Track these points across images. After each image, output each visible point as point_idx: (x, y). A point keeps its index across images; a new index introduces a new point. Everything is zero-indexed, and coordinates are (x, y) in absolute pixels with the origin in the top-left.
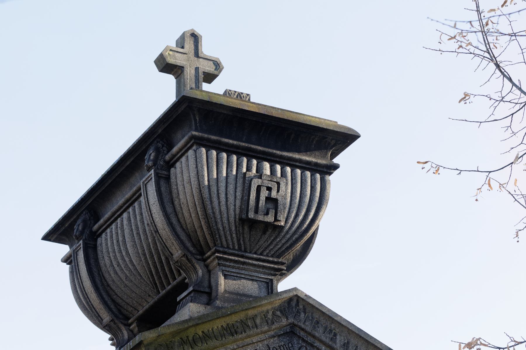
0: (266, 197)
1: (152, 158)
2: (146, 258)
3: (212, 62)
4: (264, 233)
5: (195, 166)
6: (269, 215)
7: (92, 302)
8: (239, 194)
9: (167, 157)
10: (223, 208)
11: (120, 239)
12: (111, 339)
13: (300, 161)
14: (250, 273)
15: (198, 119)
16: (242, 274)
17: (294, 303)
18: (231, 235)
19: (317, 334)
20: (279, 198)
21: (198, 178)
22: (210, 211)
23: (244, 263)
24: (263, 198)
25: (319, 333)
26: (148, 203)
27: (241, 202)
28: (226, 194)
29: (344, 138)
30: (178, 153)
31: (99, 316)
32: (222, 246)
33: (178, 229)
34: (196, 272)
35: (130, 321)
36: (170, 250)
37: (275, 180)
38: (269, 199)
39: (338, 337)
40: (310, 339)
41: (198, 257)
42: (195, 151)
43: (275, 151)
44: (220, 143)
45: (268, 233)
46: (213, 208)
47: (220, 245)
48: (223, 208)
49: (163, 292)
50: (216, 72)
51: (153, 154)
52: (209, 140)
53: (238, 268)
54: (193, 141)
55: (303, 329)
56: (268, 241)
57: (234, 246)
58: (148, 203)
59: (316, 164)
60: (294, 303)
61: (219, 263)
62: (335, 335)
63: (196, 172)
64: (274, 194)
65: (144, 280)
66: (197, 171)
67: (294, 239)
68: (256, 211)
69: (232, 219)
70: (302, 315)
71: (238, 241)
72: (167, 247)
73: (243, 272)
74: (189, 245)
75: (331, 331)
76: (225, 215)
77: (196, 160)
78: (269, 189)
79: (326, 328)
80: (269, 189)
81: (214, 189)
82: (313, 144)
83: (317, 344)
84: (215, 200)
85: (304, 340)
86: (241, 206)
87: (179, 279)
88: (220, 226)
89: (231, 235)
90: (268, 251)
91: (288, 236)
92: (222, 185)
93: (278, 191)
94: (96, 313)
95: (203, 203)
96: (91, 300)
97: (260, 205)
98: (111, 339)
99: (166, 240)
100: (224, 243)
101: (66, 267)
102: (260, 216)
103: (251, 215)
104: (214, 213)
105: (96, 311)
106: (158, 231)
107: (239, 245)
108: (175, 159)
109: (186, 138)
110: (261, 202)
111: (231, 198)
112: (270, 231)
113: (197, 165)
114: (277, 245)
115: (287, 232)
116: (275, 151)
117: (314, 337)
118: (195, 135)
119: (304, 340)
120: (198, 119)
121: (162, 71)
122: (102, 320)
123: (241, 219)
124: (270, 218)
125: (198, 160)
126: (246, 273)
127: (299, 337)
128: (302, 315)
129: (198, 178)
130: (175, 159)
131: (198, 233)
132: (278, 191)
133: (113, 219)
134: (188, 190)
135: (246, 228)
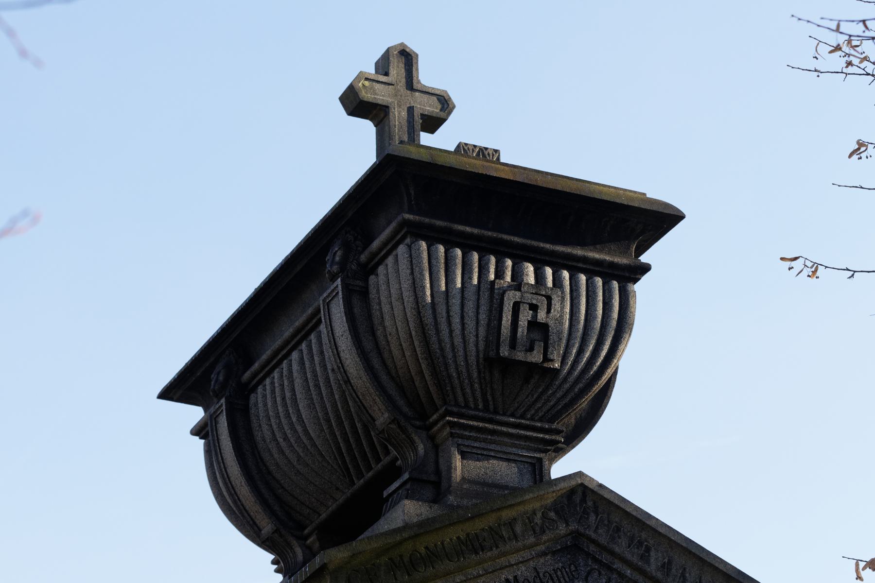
0: (529, 322)
1: (337, 259)
3: (435, 98)
5: (409, 271)
6: (535, 352)
10: (458, 340)
11: (288, 395)
13: (585, 260)
14: (504, 449)
15: (413, 192)
16: (491, 450)
17: (577, 499)
18: (472, 386)
19: (617, 549)
20: (551, 323)
21: (415, 292)
22: (435, 347)
23: (493, 432)
24: (523, 323)
25: (621, 547)
28: (462, 318)
29: (660, 220)
30: (380, 249)
31: (255, 523)
32: (457, 404)
33: (384, 378)
34: (415, 449)
35: (306, 531)
38: (533, 324)
39: (652, 553)
40: (605, 558)
41: (418, 423)
44: (450, 231)
46: (440, 341)
47: (453, 403)
48: (458, 340)
51: (339, 253)
52: (431, 227)
55: (594, 541)
56: (533, 396)
57: (476, 405)
59: (612, 265)
60: (577, 499)
61: (451, 433)
62: (648, 550)
64: (542, 316)
66: (414, 279)
67: (576, 390)
68: (513, 345)
69: (472, 359)
70: (592, 518)
71: (484, 395)
72: (365, 408)
73: (492, 447)
74: (401, 402)
75: (640, 543)
76: (461, 353)
77: (411, 261)
78: (534, 308)
79: (632, 539)
80: (534, 308)
81: (442, 309)
82: (614, 232)
83: (617, 565)
84: (444, 327)
85: (595, 560)
86: (487, 337)
88: (452, 371)
89: (472, 386)
90: (533, 412)
91: (567, 386)
92: (456, 302)
93: (549, 311)
94: (249, 519)
96: (241, 497)
99: (363, 395)
100: (461, 399)
101: (199, 444)
103: (505, 352)
104: (442, 349)
105: (249, 515)
109: (394, 225)
111: (470, 324)
113: (412, 269)
114: (548, 400)
115: (565, 379)
117: (612, 553)
119: (595, 560)
120: (413, 192)
122: (260, 530)
123: (487, 359)
124: (536, 357)
125: (414, 261)
126: (498, 448)
127: (588, 554)
128: (592, 518)
129: (415, 292)
132: (549, 311)
133: (275, 361)
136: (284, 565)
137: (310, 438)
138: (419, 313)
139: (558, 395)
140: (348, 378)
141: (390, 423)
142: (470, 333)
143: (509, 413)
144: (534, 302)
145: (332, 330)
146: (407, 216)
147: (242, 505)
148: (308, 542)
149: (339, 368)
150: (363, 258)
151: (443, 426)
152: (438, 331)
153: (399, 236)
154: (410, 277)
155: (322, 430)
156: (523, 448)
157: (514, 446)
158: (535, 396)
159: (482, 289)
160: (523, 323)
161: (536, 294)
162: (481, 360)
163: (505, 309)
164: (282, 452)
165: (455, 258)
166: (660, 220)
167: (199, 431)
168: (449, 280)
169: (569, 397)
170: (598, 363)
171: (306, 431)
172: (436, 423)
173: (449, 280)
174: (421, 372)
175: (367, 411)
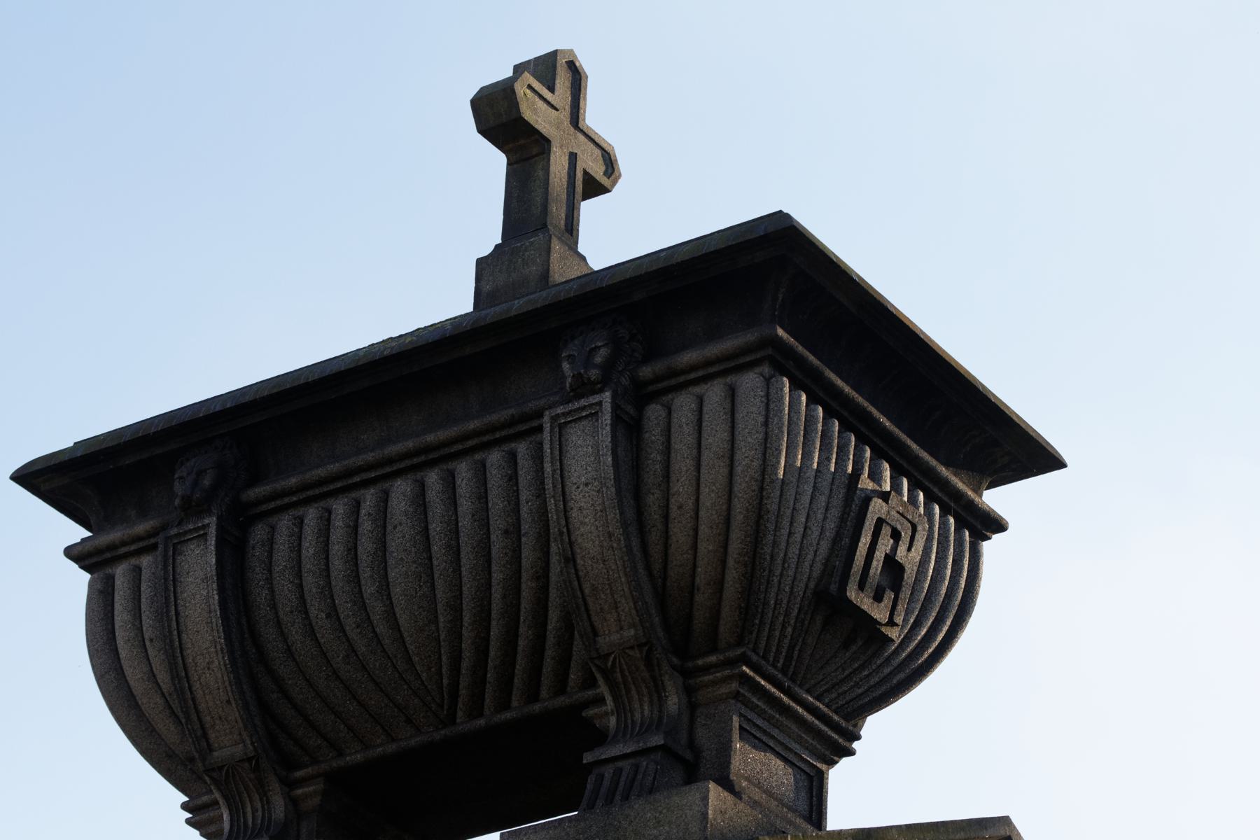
0: (886, 555)
1: (598, 359)
2: (457, 620)
3: (598, 152)
4: (846, 646)
5: (761, 419)
6: (882, 604)
7: (199, 694)
8: (831, 526)
9: (646, 372)
11: (366, 546)
12: (185, 807)
14: (786, 740)
15: (781, 296)
16: (772, 737)
18: (784, 627)
21: (764, 454)
23: (786, 710)
24: (880, 555)
26: (562, 476)
27: (832, 550)
29: (1035, 457)
30: (693, 368)
31: (205, 735)
34: (662, 701)
35: (299, 774)
36: (594, 618)
37: (910, 517)
41: (675, 660)
42: (768, 381)
43: (909, 442)
44: (818, 377)
45: (854, 648)
47: (751, 646)
49: (464, 724)
50: (604, 181)
51: (604, 352)
53: (769, 719)
54: (769, 351)
56: (844, 670)
57: (776, 659)
58: (562, 476)
61: (738, 692)
63: (761, 436)
65: (418, 676)
66: (766, 433)
67: (895, 681)
71: (791, 648)
72: (587, 610)
73: (775, 732)
77: (767, 405)
80: (896, 535)
81: (790, 493)
86: (828, 560)
87: (548, 701)
89: (784, 627)
90: (834, 695)
93: (909, 549)
94: (197, 726)
95: (758, 523)
96: (196, 686)
97: (872, 571)
98: (185, 807)
99: (594, 588)
101: (80, 580)
102: (866, 600)
105: (199, 719)
106: (574, 561)
107: (789, 658)
108: (673, 382)
109: (750, 337)
110: (874, 563)
111: (815, 532)
112: (860, 644)
113: (767, 417)
116: (909, 442)
118: (781, 338)
120: (781, 296)
121: (485, 130)
122: (211, 750)
125: (772, 406)
126: (781, 737)
129: (764, 454)
130: (673, 382)
131: (699, 598)
132: (909, 549)
133: (339, 485)
134: (713, 473)
135: (819, 620)
136: (198, 814)
137: (396, 627)
138: (762, 489)
139: (872, 682)
140: (573, 554)
141: (632, 648)
142: (811, 544)
143: (807, 686)
144: (899, 527)
145: (562, 470)
146: (780, 332)
147: (194, 699)
148: (300, 791)
149: (561, 533)
150: (646, 372)
151: (725, 680)
152: (777, 528)
153: (748, 359)
154: (762, 429)
155: (436, 621)
156: (807, 749)
157: (799, 740)
158: (847, 672)
159: (836, 482)
160: (880, 555)
161: (902, 515)
162: (809, 593)
163: (867, 523)
164: (311, 631)
165: (815, 418)
166: (1035, 457)
167: (75, 554)
168: (807, 456)
169: (883, 689)
170: (930, 650)
171: (391, 615)
172: (707, 669)
173: (807, 456)
174: (720, 584)
175: (589, 616)
